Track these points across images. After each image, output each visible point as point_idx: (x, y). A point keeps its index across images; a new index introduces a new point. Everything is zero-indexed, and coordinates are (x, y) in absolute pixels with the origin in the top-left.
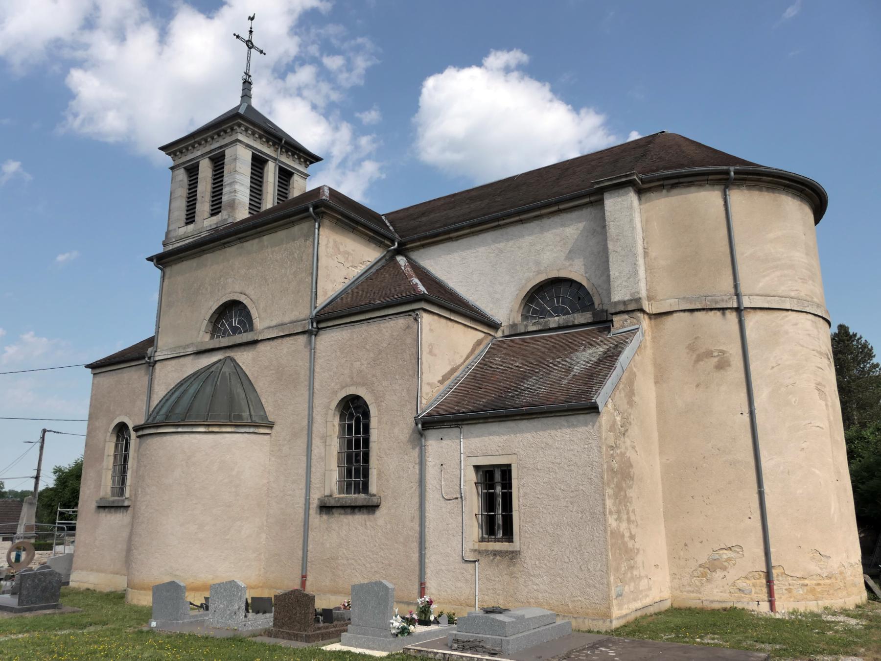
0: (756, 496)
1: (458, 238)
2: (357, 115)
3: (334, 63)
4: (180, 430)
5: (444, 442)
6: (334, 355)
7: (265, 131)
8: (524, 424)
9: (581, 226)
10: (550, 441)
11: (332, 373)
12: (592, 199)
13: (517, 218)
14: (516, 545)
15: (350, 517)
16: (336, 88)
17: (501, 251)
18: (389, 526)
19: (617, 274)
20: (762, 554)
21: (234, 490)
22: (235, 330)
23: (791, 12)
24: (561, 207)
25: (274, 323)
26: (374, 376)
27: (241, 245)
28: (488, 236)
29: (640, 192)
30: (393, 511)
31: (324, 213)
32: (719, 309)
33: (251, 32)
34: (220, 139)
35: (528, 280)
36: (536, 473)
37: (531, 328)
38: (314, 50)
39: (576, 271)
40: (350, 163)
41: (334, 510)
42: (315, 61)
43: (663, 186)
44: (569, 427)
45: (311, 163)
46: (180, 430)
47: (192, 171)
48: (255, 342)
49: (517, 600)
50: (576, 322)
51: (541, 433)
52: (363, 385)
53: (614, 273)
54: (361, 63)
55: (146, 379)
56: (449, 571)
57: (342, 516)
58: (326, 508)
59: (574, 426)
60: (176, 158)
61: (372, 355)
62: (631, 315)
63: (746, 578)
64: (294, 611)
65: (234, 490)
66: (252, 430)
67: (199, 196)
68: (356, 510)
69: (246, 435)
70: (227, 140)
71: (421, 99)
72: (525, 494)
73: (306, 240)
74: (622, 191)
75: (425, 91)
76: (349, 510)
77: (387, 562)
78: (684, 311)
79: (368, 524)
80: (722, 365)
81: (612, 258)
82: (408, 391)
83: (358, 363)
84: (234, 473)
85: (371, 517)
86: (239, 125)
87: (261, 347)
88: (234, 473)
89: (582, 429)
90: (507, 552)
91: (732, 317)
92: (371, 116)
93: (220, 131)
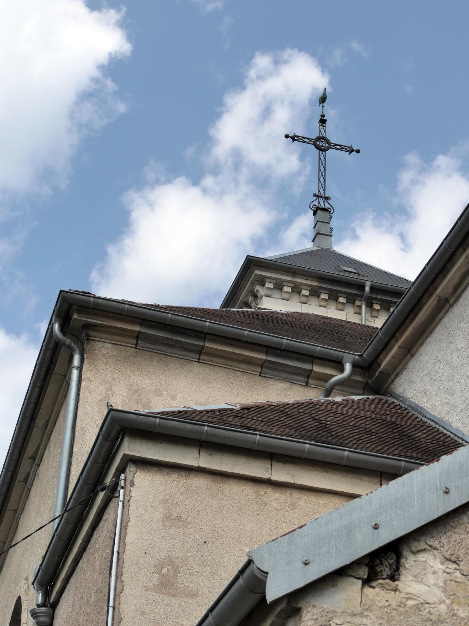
31: (88, 326)
33: (323, 121)
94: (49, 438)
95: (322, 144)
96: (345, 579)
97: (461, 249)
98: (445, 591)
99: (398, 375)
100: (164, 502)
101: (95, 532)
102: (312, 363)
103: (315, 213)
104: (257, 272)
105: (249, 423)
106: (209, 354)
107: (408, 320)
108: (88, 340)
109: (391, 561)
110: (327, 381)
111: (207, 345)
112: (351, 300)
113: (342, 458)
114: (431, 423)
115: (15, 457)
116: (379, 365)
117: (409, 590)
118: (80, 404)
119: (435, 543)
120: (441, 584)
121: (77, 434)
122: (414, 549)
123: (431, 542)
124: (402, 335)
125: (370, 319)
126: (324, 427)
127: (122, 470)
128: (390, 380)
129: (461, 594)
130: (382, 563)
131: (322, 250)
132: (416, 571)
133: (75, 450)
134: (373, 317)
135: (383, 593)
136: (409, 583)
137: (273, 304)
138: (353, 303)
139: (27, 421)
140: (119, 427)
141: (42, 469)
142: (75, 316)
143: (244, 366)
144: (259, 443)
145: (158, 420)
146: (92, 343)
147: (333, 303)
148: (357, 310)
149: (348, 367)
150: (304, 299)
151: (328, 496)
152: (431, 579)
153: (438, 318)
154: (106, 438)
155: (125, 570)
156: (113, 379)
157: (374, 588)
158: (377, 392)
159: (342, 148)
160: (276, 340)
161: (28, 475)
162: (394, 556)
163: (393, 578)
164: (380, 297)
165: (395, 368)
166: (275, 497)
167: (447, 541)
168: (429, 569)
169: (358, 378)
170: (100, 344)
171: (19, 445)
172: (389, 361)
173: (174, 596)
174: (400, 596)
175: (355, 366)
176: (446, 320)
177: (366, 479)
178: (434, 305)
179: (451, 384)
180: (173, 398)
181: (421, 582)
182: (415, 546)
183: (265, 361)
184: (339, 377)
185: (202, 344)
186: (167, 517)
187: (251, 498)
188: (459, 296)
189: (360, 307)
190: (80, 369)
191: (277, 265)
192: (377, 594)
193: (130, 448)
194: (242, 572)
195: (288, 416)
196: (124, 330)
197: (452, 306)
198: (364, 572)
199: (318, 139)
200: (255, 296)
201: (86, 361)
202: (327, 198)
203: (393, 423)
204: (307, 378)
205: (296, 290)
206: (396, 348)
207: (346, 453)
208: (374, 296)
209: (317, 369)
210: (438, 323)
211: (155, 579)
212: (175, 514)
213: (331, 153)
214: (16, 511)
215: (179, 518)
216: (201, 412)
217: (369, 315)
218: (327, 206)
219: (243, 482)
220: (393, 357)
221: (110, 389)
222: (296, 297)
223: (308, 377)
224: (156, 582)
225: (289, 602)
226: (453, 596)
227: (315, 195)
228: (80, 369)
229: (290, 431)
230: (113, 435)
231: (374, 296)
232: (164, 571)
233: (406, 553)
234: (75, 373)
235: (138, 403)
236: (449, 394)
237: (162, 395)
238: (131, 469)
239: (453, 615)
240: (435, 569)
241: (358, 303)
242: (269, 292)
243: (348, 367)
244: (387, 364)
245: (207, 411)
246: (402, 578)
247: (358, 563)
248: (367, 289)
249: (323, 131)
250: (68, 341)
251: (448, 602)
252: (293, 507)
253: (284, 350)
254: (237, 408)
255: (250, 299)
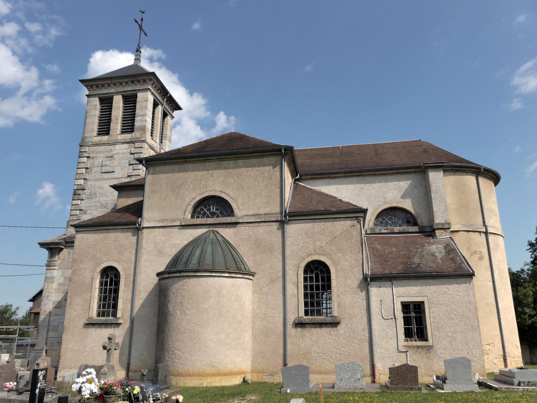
0: (497, 320)
1: (334, 178)
2: (43, 65)
3: (34, 27)
4: (213, 274)
5: (381, 289)
6: (300, 237)
8: (430, 281)
9: (409, 182)
10: (447, 291)
11: (300, 247)
12: (417, 170)
13: (373, 173)
14: (430, 343)
15: (319, 329)
16: (32, 44)
18: (347, 334)
19: (437, 210)
20: (501, 347)
21: (242, 312)
22: (213, 215)
23: (308, 68)
24: (399, 171)
25: (251, 213)
26: (331, 250)
27: (220, 162)
28: (354, 179)
29: (444, 171)
30: (349, 325)
32: (478, 232)
33: (142, 20)
34: (133, 85)
35: (379, 206)
36: (439, 306)
37: (383, 231)
38: (19, 15)
39: (407, 205)
40: (34, 95)
41: (306, 326)
42: (18, 22)
43: (452, 170)
44: (456, 284)
45: (176, 110)
46: (213, 274)
47: (106, 103)
48: (236, 224)
49: (432, 370)
50: (410, 231)
51: (441, 286)
52: (324, 255)
53: (435, 209)
54: (53, 32)
55: (134, 239)
56: (389, 357)
57: (313, 329)
58: (299, 324)
59: (459, 284)
60: (91, 89)
61: (329, 238)
63: (496, 358)
64: (406, 376)
67: (112, 118)
68: (323, 325)
70: (138, 87)
71: (89, 65)
72: (434, 317)
73: (274, 168)
74: (438, 170)
75: (92, 60)
76: (318, 325)
77: (347, 354)
78: (464, 231)
79: (332, 333)
80: (481, 258)
81: (434, 202)
82: (356, 260)
83: (320, 243)
84: (242, 302)
85: (334, 329)
86: (150, 80)
87: (240, 228)
89: (464, 285)
90: (425, 346)
91: (483, 235)
92: (55, 68)
93: (135, 80)
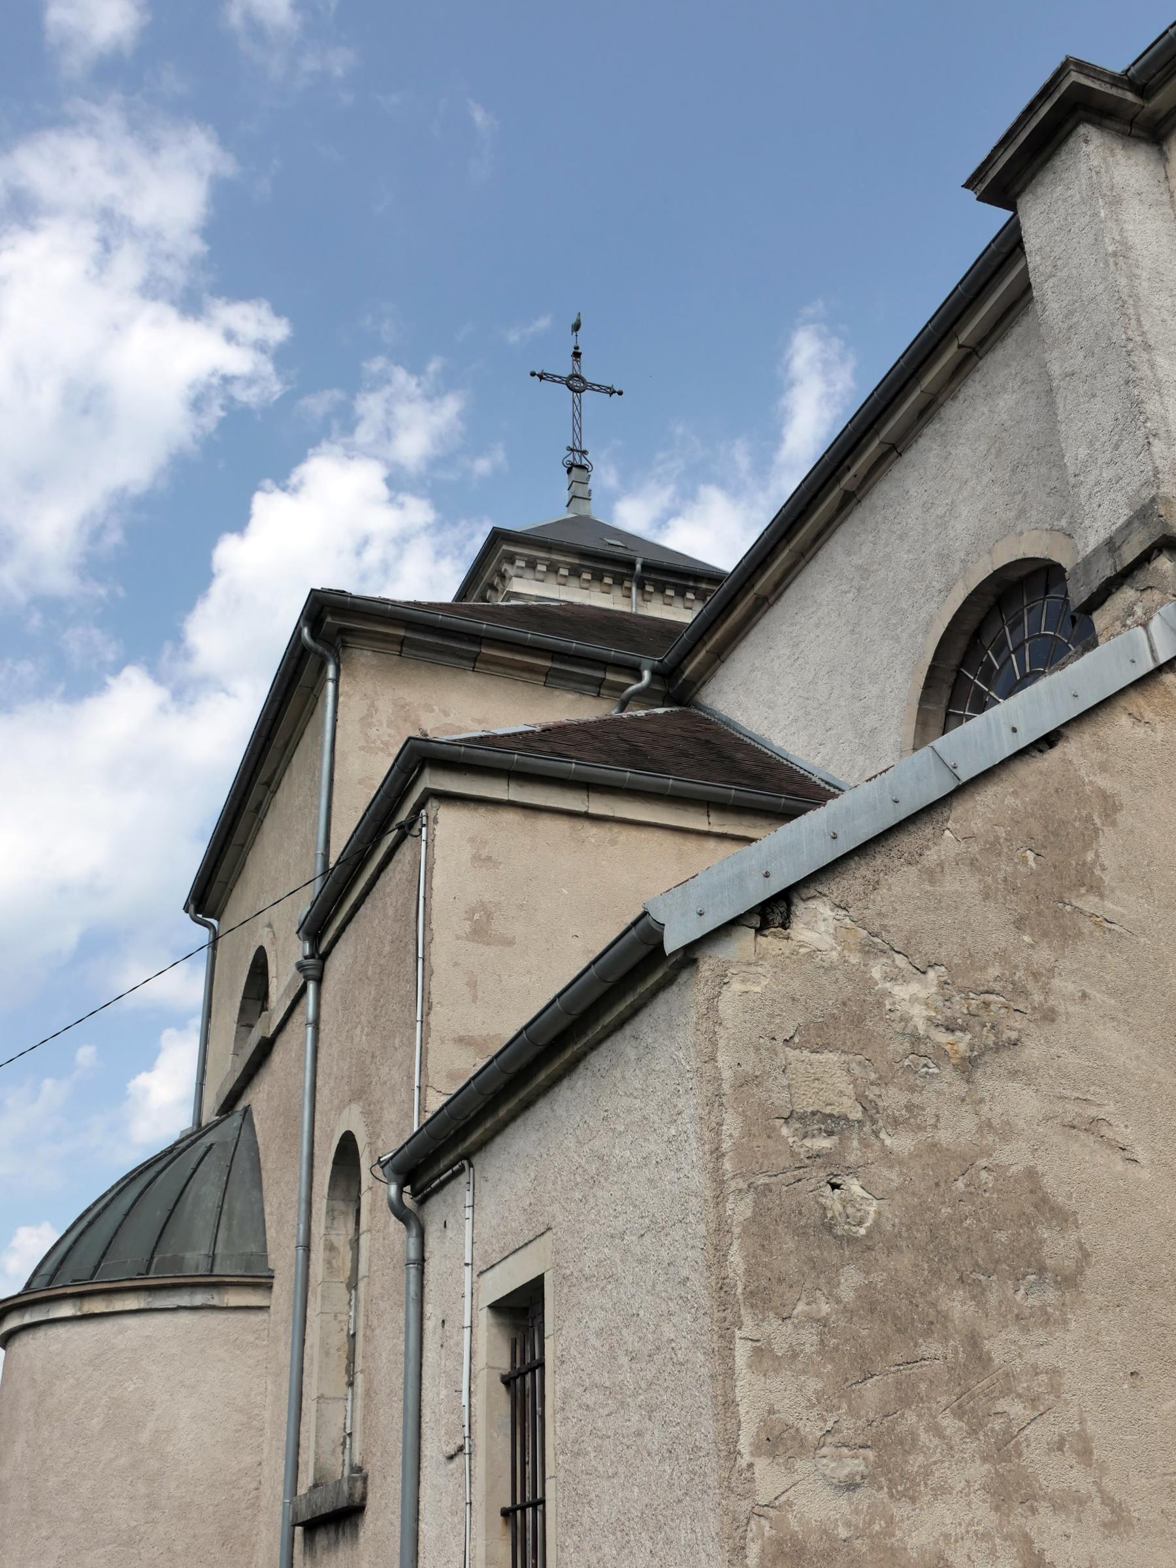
7: (584, 554)
17: (865, 572)
21: (142, 1489)
31: (343, 631)
33: (577, 355)
62: (1141, 577)
65: (142, 1489)
66: (199, 1299)
69: (185, 1318)
84: (145, 1437)
88: (145, 1437)
93: (484, 591)
94: (290, 761)
95: (577, 384)
96: (739, 928)
97: (784, 541)
98: (835, 938)
99: (704, 683)
100: (472, 840)
101: (383, 875)
102: (605, 670)
103: (569, 471)
104: (505, 547)
105: (558, 749)
106: (486, 662)
107: (719, 621)
108: (344, 647)
109: (782, 909)
110: (623, 691)
111: (483, 651)
112: (619, 581)
113: (666, 787)
114: (749, 741)
115: (244, 783)
116: (683, 672)
117: (801, 938)
118: (339, 723)
119: (825, 891)
120: (832, 931)
121: (337, 758)
122: (804, 896)
123: (821, 888)
124: (711, 638)
125: (641, 603)
126: (635, 750)
127: (421, 805)
128: (695, 689)
129: (851, 940)
130: (773, 913)
131: (579, 517)
132: (806, 918)
133: (336, 777)
134: (644, 600)
135: (775, 941)
136: (800, 931)
137: (529, 587)
138: (621, 584)
139: (262, 740)
140: (419, 757)
141: (281, 796)
142: (329, 619)
143: (526, 675)
144: (575, 773)
145: (463, 749)
146: (349, 651)
147: (597, 584)
148: (626, 593)
149: (646, 675)
150: (562, 580)
151: (651, 829)
152: (822, 927)
153: (755, 619)
154: (402, 770)
155: (434, 917)
156: (376, 693)
157: (766, 936)
158: (678, 703)
159: (602, 389)
160: (563, 644)
161: (260, 804)
162: (784, 904)
163: (784, 926)
164: (653, 576)
165: (700, 677)
166: (593, 832)
167: (837, 887)
168: (819, 916)
169: (658, 687)
170: (358, 652)
171: (250, 769)
172: (696, 667)
173: (488, 944)
174: (792, 944)
175: (654, 673)
176: (764, 622)
177: (692, 809)
178: (750, 604)
179: (771, 696)
180: (446, 714)
181: (812, 929)
182: (806, 893)
183: (551, 669)
184: (636, 686)
185: (477, 650)
186: (476, 858)
187: (567, 834)
188: (780, 595)
189: (630, 589)
190: (336, 681)
191: (529, 539)
192: (770, 943)
193: (431, 780)
194: (634, 924)
195: (594, 737)
196: (387, 635)
197: (771, 605)
198: (756, 921)
199: (572, 377)
200: (503, 577)
201: (342, 673)
202: (584, 452)
203: (708, 742)
204: (598, 688)
205: (553, 568)
206: (703, 653)
207: (671, 781)
208: (646, 575)
209: (611, 677)
210: (755, 624)
211: (467, 926)
212: (484, 853)
213: (587, 394)
214: (243, 846)
215: (489, 858)
216: (502, 736)
217: (640, 598)
218: (584, 462)
219: (557, 816)
220: (699, 663)
221: (372, 705)
222: (552, 578)
223: (600, 686)
224: (468, 930)
225: (685, 953)
226: (844, 943)
227: (569, 449)
228: (336, 681)
229: (604, 757)
230: (410, 766)
231: (646, 575)
232: (476, 917)
233: (795, 900)
234: (330, 686)
235: (405, 720)
236: (769, 707)
237: (433, 711)
238: (432, 804)
239: (845, 962)
240: (825, 916)
241: (627, 584)
242: (520, 572)
243: (646, 675)
244: (692, 671)
245: (508, 735)
246: (793, 925)
247: (750, 912)
248: (638, 567)
249: (577, 368)
250: (320, 649)
251: (839, 948)
252: (613, 842)
253: (573, 656)
254: (538, 729)
255: (496, 580)
